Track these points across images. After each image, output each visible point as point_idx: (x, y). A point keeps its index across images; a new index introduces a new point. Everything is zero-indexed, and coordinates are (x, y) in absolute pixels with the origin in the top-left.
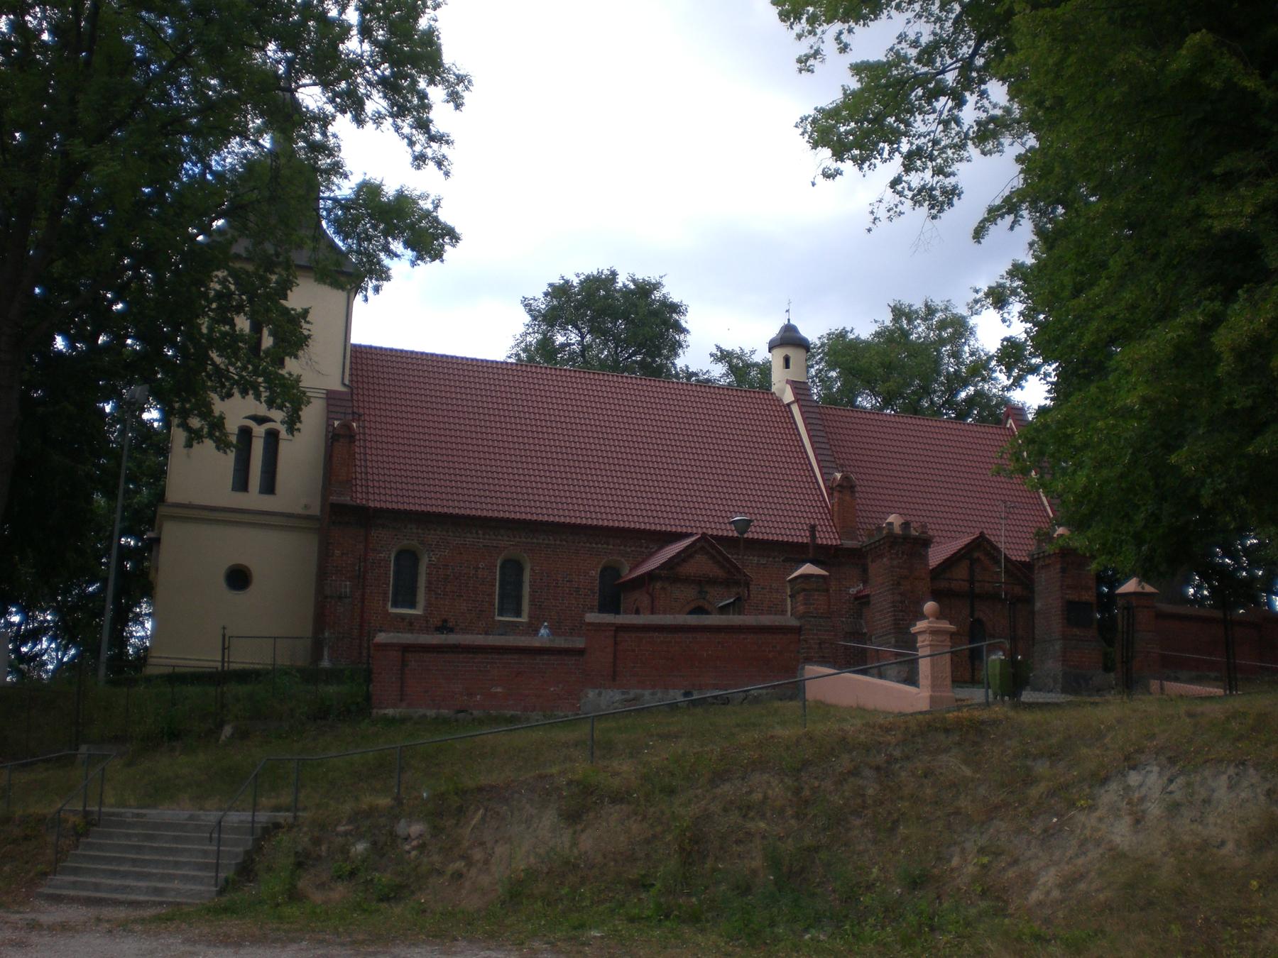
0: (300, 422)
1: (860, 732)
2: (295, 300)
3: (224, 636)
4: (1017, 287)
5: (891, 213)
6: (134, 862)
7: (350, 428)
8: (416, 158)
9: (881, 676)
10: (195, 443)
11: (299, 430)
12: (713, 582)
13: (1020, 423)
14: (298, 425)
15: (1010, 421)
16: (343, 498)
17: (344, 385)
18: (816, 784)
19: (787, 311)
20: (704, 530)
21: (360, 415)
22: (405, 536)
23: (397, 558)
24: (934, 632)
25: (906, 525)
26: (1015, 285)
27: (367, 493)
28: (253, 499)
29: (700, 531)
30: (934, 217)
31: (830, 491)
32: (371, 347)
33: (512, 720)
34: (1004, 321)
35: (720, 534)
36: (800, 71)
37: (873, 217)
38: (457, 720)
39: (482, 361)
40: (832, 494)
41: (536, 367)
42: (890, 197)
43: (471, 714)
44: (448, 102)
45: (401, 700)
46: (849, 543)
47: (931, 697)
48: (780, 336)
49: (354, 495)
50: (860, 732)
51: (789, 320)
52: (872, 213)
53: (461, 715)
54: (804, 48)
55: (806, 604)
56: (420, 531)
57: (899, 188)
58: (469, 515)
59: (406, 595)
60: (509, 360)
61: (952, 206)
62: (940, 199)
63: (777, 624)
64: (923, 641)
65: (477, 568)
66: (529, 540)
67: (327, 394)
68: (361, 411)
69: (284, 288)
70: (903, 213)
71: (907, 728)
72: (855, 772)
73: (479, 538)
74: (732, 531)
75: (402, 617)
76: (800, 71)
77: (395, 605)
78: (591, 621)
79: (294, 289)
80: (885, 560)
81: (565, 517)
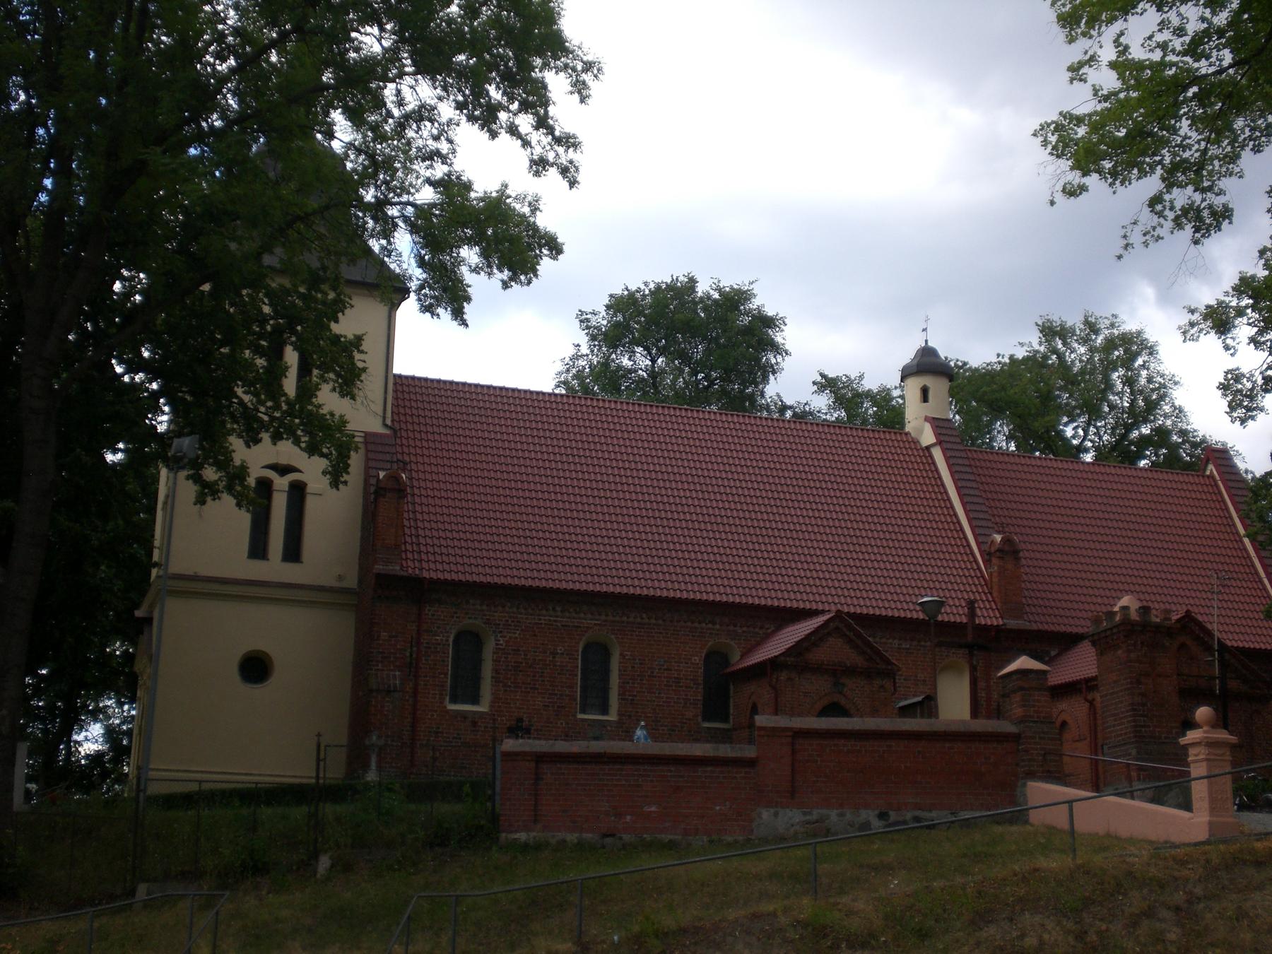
0: (348, 473)
1: (1149, 864)
2: (345, 327)
3: (319, 746)
4: (1247, 307)
5: (1147, 237)
7: (397, 479)
8: (533, 162)
9: (1133, 798)
10: (209, 499)
11: (345, 483)
12: (851, 671)
13: (1223, 469)
14: (345, 477)
15: (1211, 467)
16: (391, 568)
17: (385, 425)
18: (1104, 927)
19: (924, 330)
20: (839, 607)
21: (405, 463)
22: (467, 614)
23: (456, 641)
24: (1211, 744)
25: (1145, 610)
26: (1243, 303)
27: (421, 561)
28: (274, 568)
29: (833, 608)
30: (1196, 242)
31: (986, 557)
32: (413, 378)
33: (672, 845)
34: (1227, 348)
35: (865, 612)
36: (1072, 81)
37: (1125, 242)
38: (603, 847)
39: (525, 391)
40: (990, 561)
41: (592, 399)
42: (1147, 218)
43: (621, 838)
44: (572, 93)
45: (535, 821)
46: (1013, 623)
47: (1210, 823)
48: (916, 362)
49: (404, 563)
50: (1149, 864)
51: (926, 341)
52: (1125, 237)
53: (608, 840)
54: (1075, 52)
55: (1024, 706)
56: (484, 607)
57: (1159, 207)
58: (559, 588)
59: (467, 688)
60: (557, 391)
61: (1220, 230)
62: (1208, 221)
63: (990, 730)
64: (1196, 755)
65: (554, 654)
66: (617, 618)
67: (365, 437)
68: (407, 458)
69: (336, 309)
70: (1162, 238)
71: (1207, 861)
72: (1149, 913)
73: (557, 617)
74: (917, 611)
75: (463, 716)
76: (1072, 81)
77: (454, 700)
78: (764, 725)
79: (347, 311)
80: (1119, 652)
81: (594, 584)
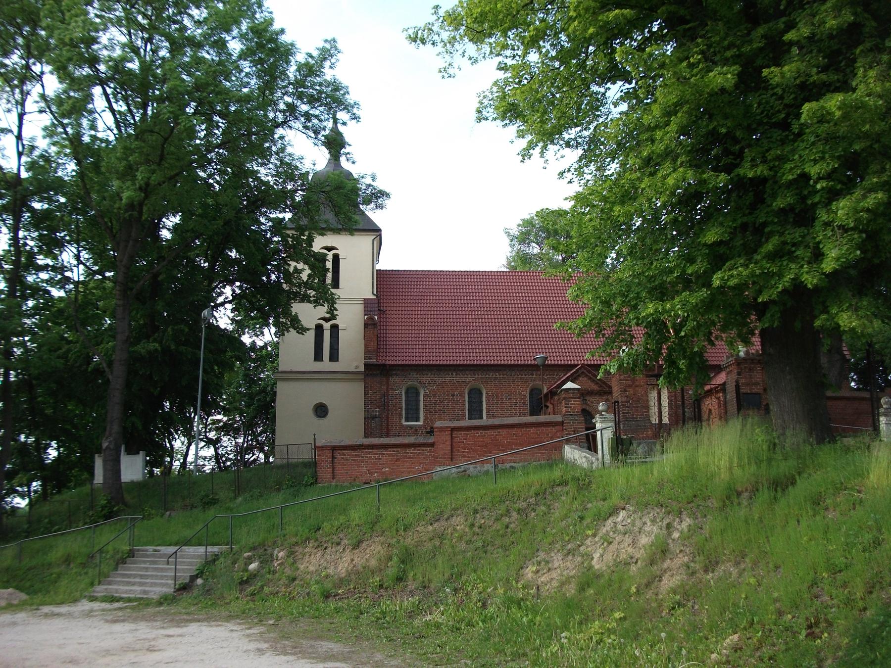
6: (141, 576)
17: (374, 294)
23: (406, 393)
59: (413, 414)
68: (385, 309)
75: (411, 427)
77: (407, 420)
